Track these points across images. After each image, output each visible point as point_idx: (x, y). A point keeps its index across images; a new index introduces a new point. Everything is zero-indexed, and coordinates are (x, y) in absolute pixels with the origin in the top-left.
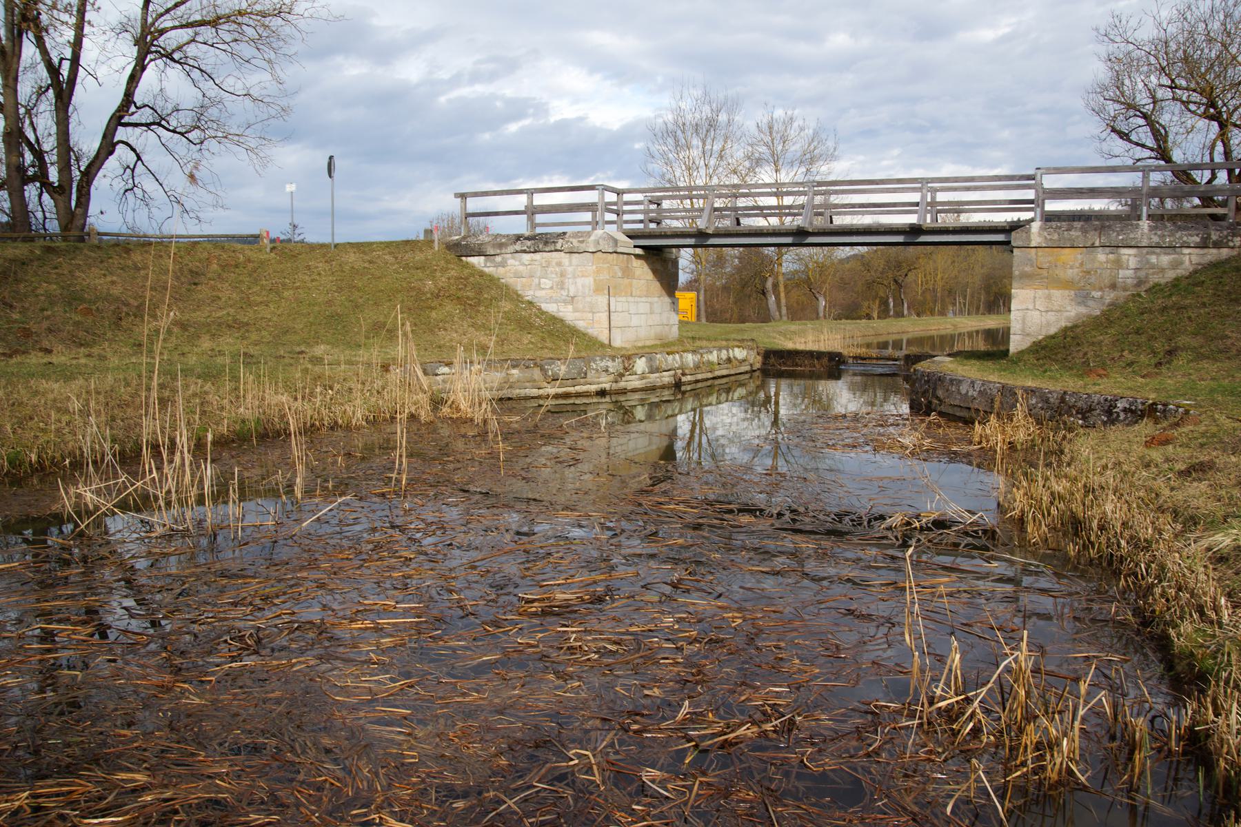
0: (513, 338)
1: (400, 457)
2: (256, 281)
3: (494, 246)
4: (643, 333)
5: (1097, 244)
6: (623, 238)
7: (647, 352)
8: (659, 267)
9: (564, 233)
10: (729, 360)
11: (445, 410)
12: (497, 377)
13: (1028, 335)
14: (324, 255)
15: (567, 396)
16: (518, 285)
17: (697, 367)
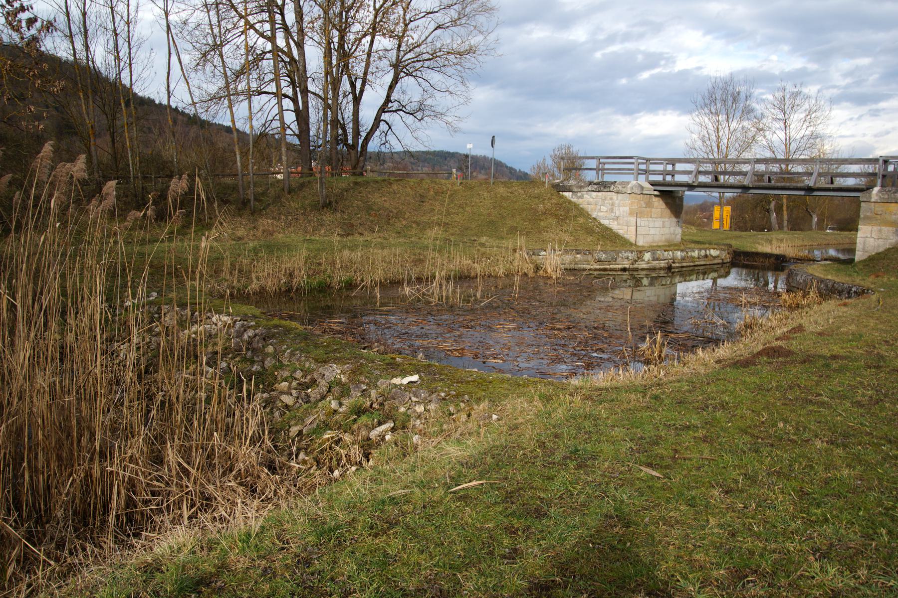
0: (582, 238)
1: (516, 287)
2: (452, 201)
3: (577, 187)
4: (657, 238)
6: (648, 186)
7: (653, 249)
8: (669, 201)
9: (615, 182)
10: (706, 256)
11: (541, 272)
12: (568, 258)
13: (866, 252)
14: (487, 188)
15: (605, 270)
16: (589, 208)
17: (683, 259)
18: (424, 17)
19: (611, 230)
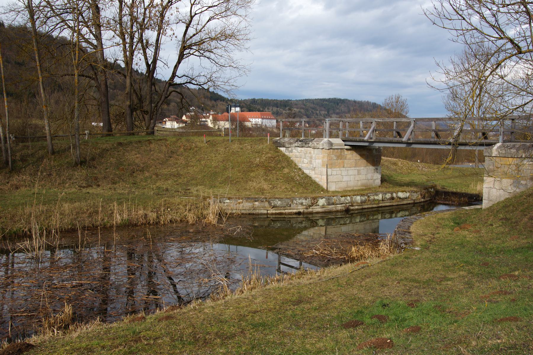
5: (524, 156)
10: (392, 198)
13: (491, 200)
16: (296, 160)
17: (363, 202)
18: (206, 10)
19: (310, 178)
